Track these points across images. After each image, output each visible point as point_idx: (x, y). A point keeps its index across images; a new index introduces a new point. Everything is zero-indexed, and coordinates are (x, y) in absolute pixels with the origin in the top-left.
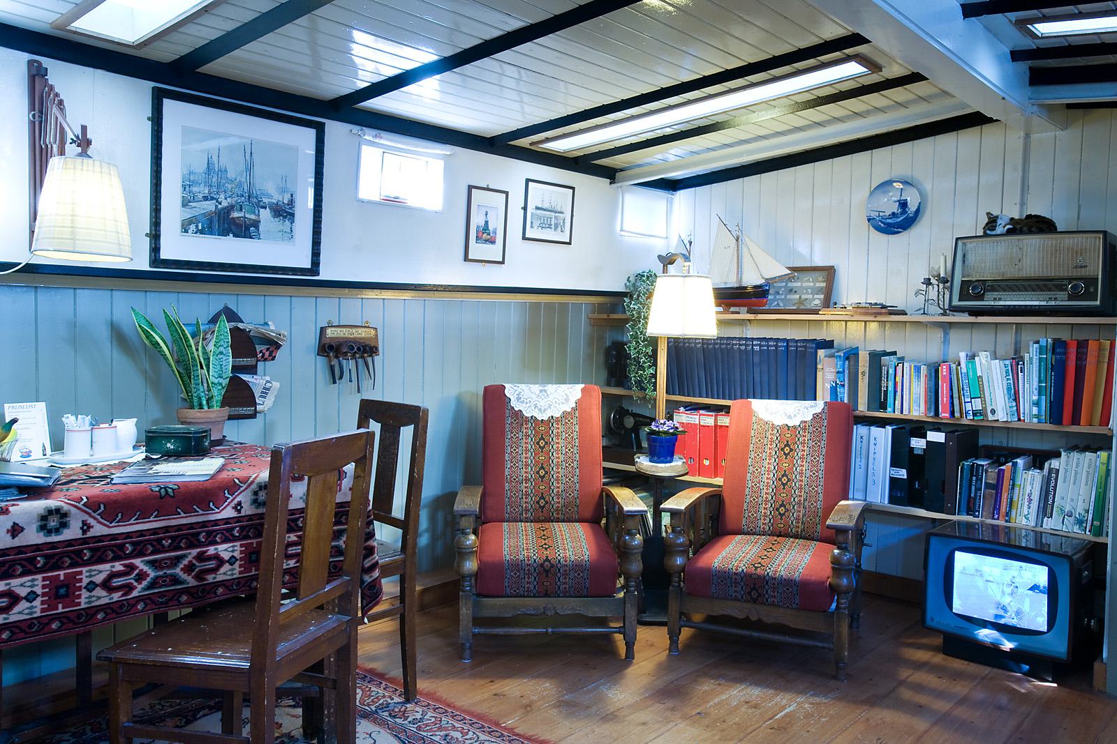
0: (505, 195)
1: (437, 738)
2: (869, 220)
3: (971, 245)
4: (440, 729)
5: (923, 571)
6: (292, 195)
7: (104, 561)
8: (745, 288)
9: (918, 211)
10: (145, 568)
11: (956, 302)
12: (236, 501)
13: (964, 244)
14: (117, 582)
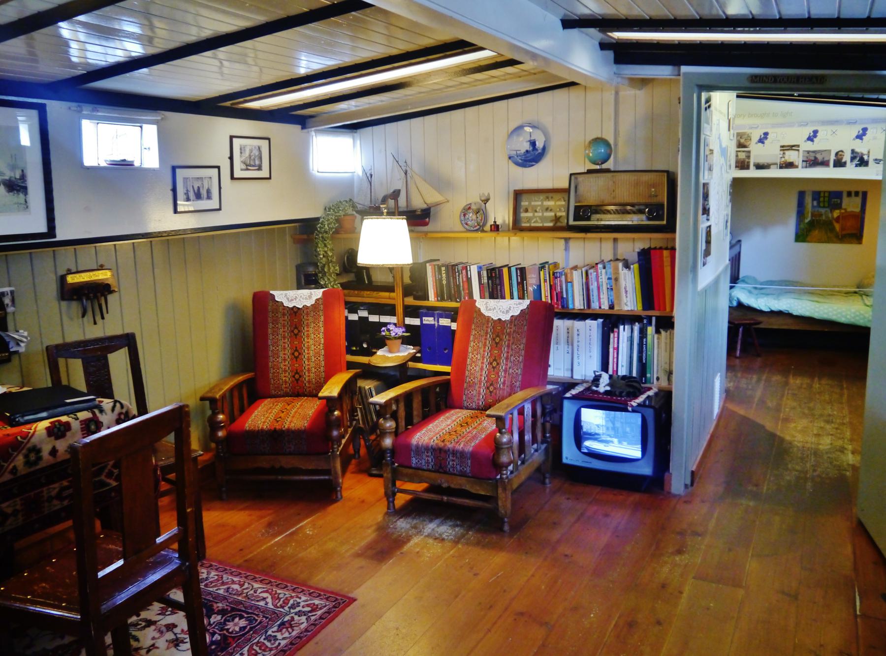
0: (236, 176)
1: (221, 592)
2: (510, 158)
3: (581, 178)
4: (223, 584)
5: (229, 161)
6: (23, 171)
7: (54, 482)
8: (415, 211)
9: (544, 149)
10: (108, 481)
11: (571, 222)
12: (11, 467)
13: (576, 178)
14: (66, 493)
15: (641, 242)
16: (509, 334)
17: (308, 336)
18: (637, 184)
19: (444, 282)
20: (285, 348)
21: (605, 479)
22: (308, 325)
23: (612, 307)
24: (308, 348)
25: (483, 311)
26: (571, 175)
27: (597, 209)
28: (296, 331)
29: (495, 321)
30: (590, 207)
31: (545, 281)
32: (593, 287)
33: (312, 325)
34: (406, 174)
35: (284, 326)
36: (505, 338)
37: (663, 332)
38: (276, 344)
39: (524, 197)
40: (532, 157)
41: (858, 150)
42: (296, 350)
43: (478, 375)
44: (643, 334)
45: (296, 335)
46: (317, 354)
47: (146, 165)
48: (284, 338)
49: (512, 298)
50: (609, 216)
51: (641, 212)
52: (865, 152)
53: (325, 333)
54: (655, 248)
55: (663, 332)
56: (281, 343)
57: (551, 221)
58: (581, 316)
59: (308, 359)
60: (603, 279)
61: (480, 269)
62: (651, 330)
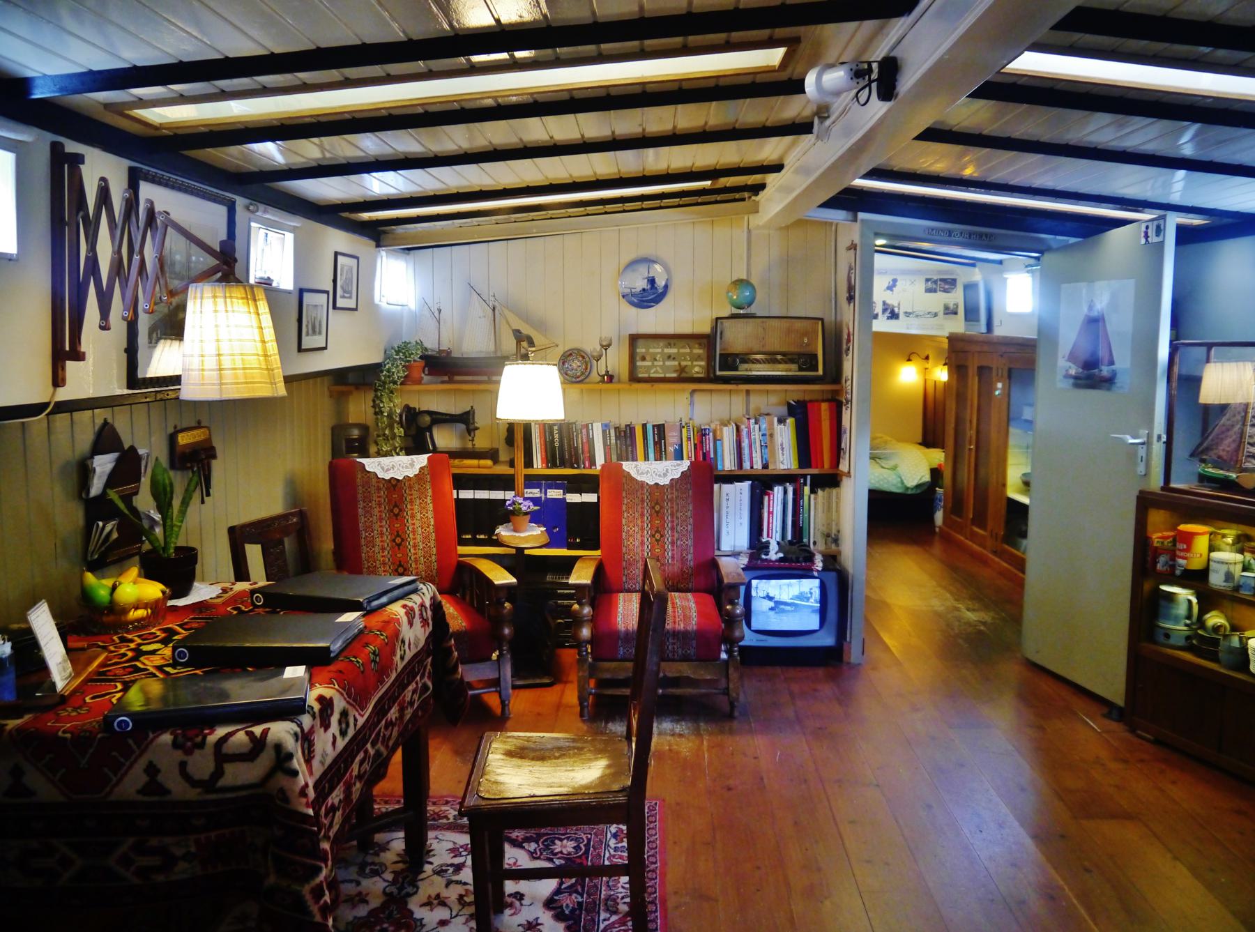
9: (666, 287)
15: (795, 392)
16: (671, 500)
17: (413, 516)
18: (789, 331)
19: (557, 444)
20: (382, 534)
21: (787, 658)
22: (411, 502)
23: (765, 466)
24: (414, 532)
25: (634, 474)
26: (717, 319)
27: (745, 358)
28: (396, 511)
29: (651, 486)
30: (737, 355)
31: (689, 439)
32: (745, 444)
33: (418, 502)
34: (494, 309)
35: (380, 505)
36: (667, 505)
37: (820, 492)
38: (370, 528)
39: (640, 342)
40: (650, 296)
41: (889, 302)
42: (398, 535)
43: (639, 550)
44: (798, 496)
45: (396, 515)
46: (426, 538)
47: (282, 287)
48: (381, 519)
49: (646, 458)
50: (758, 366)
51: (792, 361)
52: (896, 304)
53: (435, 511)
54: (811, 401)
55: (820, 492)
56: (376, 526)
57: (675, 371)
58: (730, 478)
59: (415, 547)
60: (756, 436)
61: (606, 428)
62: (807, 489)
